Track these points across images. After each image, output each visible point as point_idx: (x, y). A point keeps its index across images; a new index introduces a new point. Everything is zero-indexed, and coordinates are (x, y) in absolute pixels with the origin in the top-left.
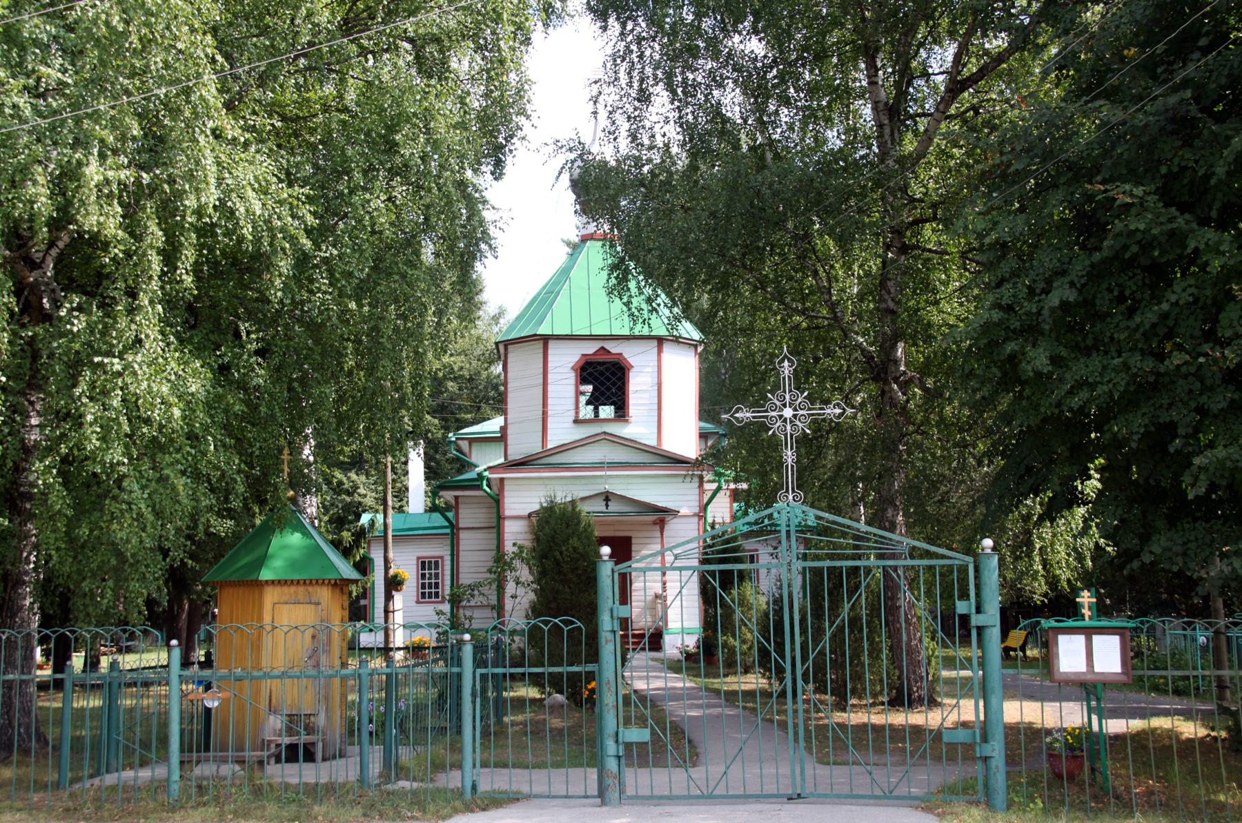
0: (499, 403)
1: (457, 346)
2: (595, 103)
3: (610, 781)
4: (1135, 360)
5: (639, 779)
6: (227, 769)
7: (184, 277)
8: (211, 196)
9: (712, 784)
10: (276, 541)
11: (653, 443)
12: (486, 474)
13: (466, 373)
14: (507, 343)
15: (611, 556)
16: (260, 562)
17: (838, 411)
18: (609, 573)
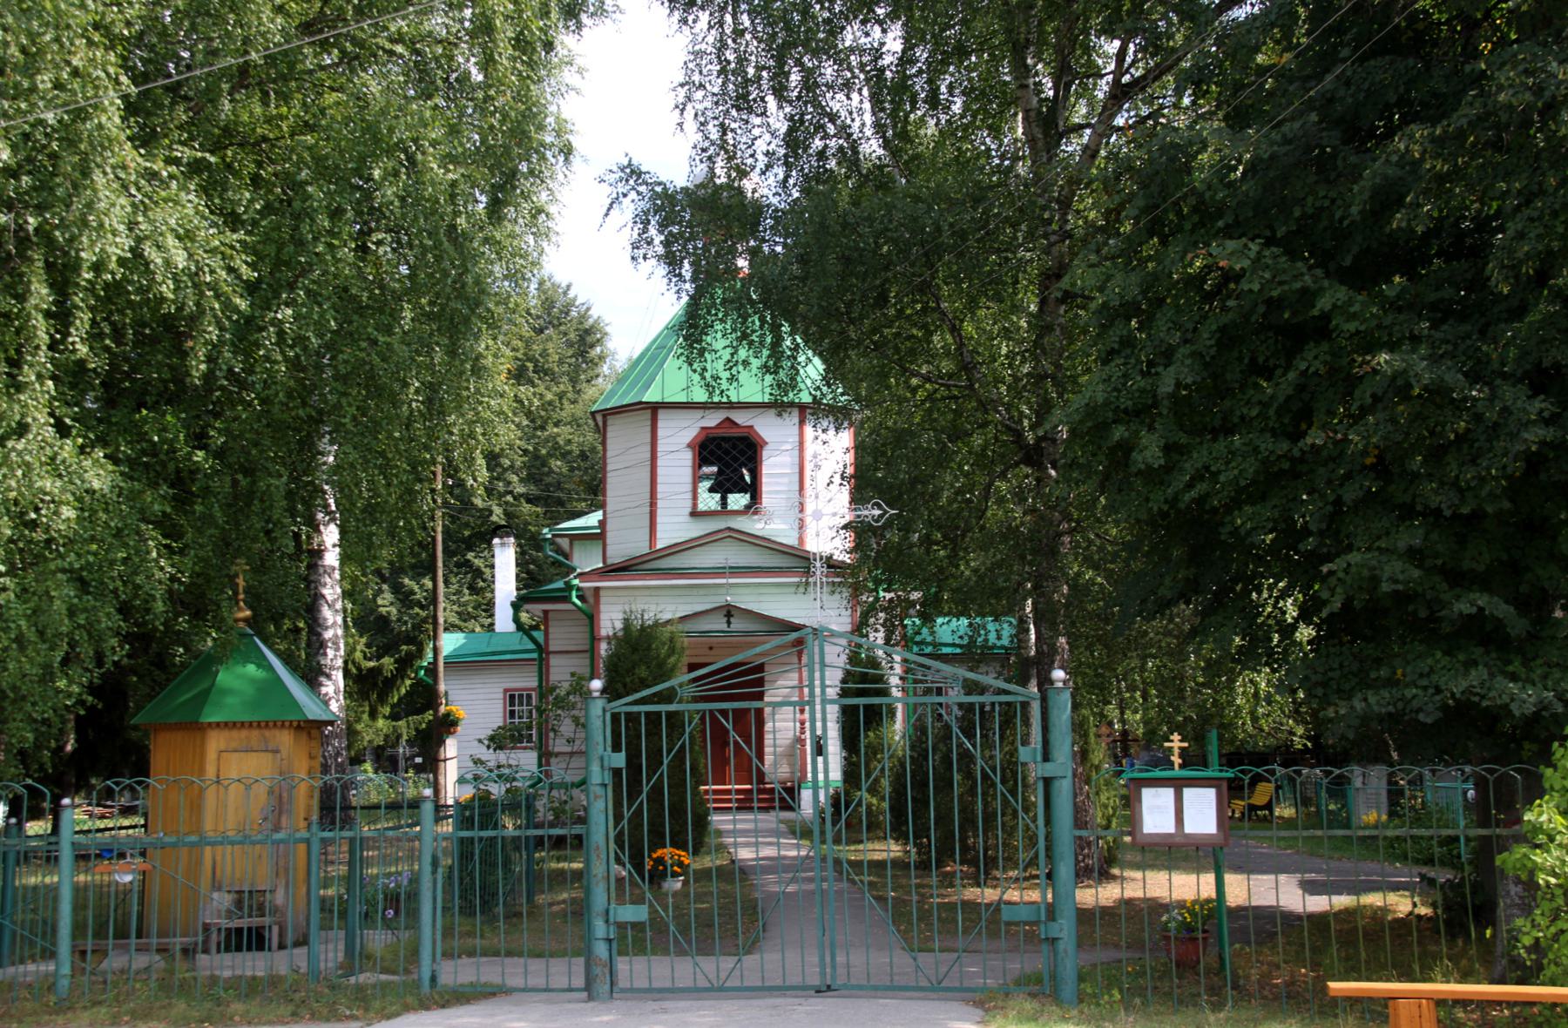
0: (595, 493)
1: (564, 414)
2: (682, 111)
3: (597, 970)
4: (1267, 444)
5: (631, 969)
6: (141, 961)
7: (78, 346)
8: (118, 246)
9: (723, 975)
10: (224, 677)
13: (575, 449)
14: (607, 413)
15: (604, 691)
16: (202, 699)
17: (877, 512)
18: (600, 712)
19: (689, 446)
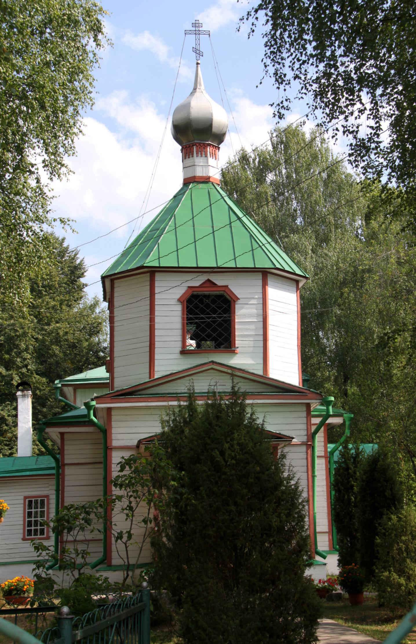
11: (261, 373)
12: (94, 403)
19: (179, 300)
